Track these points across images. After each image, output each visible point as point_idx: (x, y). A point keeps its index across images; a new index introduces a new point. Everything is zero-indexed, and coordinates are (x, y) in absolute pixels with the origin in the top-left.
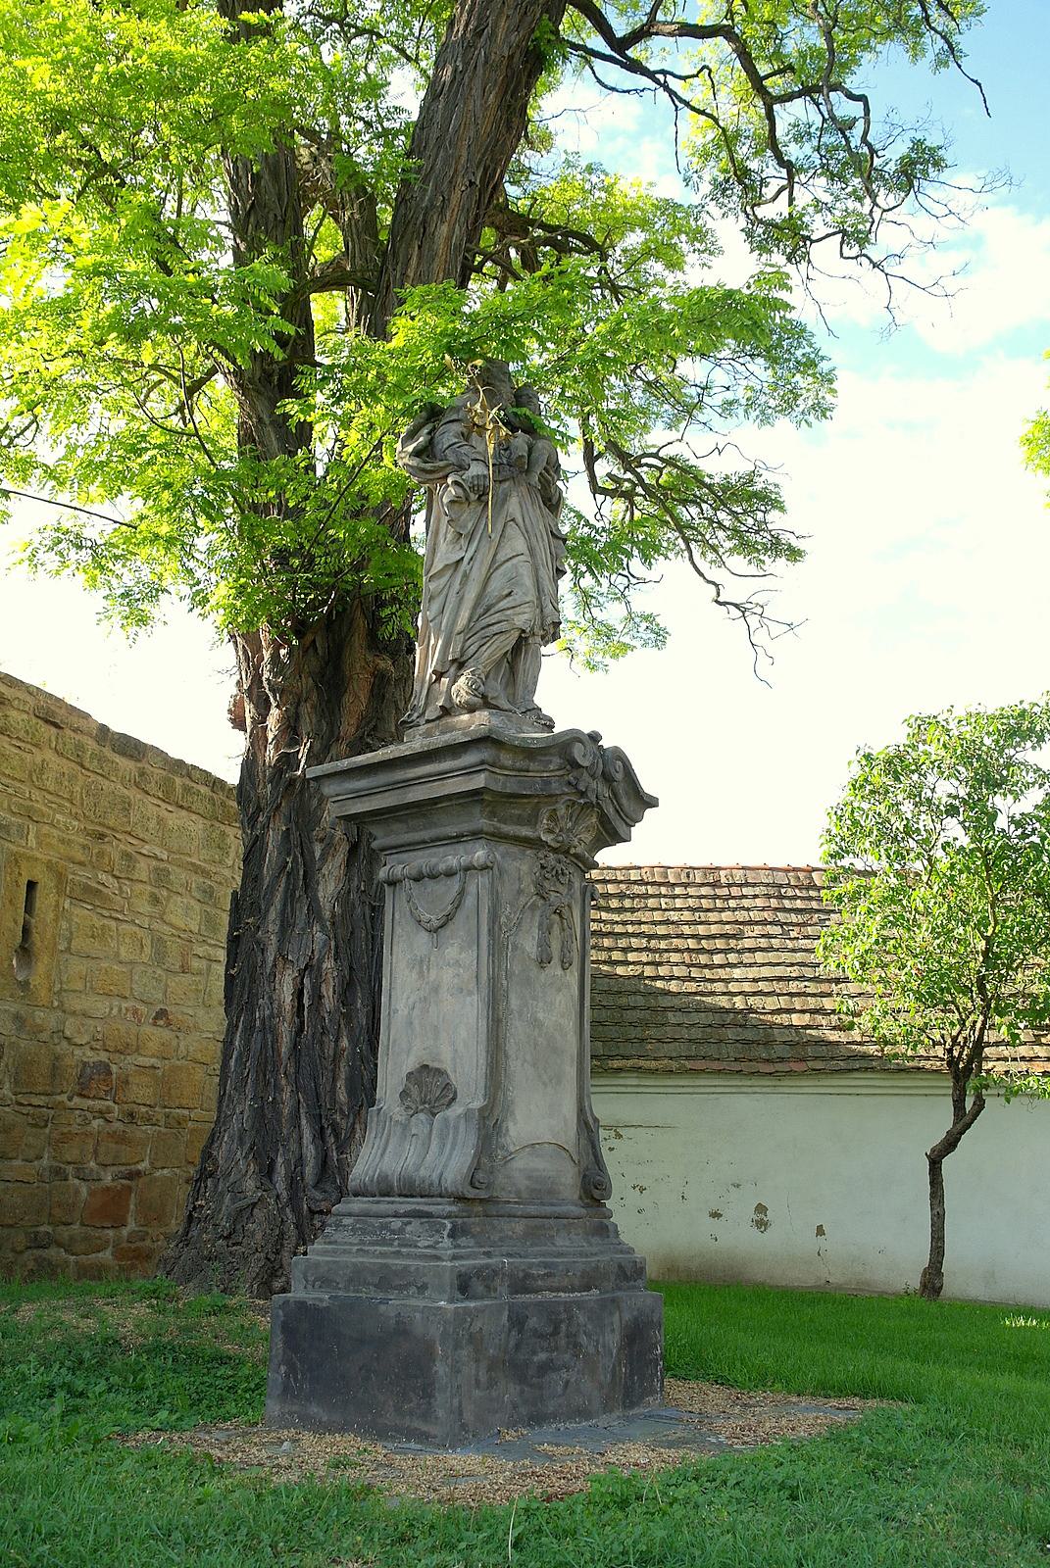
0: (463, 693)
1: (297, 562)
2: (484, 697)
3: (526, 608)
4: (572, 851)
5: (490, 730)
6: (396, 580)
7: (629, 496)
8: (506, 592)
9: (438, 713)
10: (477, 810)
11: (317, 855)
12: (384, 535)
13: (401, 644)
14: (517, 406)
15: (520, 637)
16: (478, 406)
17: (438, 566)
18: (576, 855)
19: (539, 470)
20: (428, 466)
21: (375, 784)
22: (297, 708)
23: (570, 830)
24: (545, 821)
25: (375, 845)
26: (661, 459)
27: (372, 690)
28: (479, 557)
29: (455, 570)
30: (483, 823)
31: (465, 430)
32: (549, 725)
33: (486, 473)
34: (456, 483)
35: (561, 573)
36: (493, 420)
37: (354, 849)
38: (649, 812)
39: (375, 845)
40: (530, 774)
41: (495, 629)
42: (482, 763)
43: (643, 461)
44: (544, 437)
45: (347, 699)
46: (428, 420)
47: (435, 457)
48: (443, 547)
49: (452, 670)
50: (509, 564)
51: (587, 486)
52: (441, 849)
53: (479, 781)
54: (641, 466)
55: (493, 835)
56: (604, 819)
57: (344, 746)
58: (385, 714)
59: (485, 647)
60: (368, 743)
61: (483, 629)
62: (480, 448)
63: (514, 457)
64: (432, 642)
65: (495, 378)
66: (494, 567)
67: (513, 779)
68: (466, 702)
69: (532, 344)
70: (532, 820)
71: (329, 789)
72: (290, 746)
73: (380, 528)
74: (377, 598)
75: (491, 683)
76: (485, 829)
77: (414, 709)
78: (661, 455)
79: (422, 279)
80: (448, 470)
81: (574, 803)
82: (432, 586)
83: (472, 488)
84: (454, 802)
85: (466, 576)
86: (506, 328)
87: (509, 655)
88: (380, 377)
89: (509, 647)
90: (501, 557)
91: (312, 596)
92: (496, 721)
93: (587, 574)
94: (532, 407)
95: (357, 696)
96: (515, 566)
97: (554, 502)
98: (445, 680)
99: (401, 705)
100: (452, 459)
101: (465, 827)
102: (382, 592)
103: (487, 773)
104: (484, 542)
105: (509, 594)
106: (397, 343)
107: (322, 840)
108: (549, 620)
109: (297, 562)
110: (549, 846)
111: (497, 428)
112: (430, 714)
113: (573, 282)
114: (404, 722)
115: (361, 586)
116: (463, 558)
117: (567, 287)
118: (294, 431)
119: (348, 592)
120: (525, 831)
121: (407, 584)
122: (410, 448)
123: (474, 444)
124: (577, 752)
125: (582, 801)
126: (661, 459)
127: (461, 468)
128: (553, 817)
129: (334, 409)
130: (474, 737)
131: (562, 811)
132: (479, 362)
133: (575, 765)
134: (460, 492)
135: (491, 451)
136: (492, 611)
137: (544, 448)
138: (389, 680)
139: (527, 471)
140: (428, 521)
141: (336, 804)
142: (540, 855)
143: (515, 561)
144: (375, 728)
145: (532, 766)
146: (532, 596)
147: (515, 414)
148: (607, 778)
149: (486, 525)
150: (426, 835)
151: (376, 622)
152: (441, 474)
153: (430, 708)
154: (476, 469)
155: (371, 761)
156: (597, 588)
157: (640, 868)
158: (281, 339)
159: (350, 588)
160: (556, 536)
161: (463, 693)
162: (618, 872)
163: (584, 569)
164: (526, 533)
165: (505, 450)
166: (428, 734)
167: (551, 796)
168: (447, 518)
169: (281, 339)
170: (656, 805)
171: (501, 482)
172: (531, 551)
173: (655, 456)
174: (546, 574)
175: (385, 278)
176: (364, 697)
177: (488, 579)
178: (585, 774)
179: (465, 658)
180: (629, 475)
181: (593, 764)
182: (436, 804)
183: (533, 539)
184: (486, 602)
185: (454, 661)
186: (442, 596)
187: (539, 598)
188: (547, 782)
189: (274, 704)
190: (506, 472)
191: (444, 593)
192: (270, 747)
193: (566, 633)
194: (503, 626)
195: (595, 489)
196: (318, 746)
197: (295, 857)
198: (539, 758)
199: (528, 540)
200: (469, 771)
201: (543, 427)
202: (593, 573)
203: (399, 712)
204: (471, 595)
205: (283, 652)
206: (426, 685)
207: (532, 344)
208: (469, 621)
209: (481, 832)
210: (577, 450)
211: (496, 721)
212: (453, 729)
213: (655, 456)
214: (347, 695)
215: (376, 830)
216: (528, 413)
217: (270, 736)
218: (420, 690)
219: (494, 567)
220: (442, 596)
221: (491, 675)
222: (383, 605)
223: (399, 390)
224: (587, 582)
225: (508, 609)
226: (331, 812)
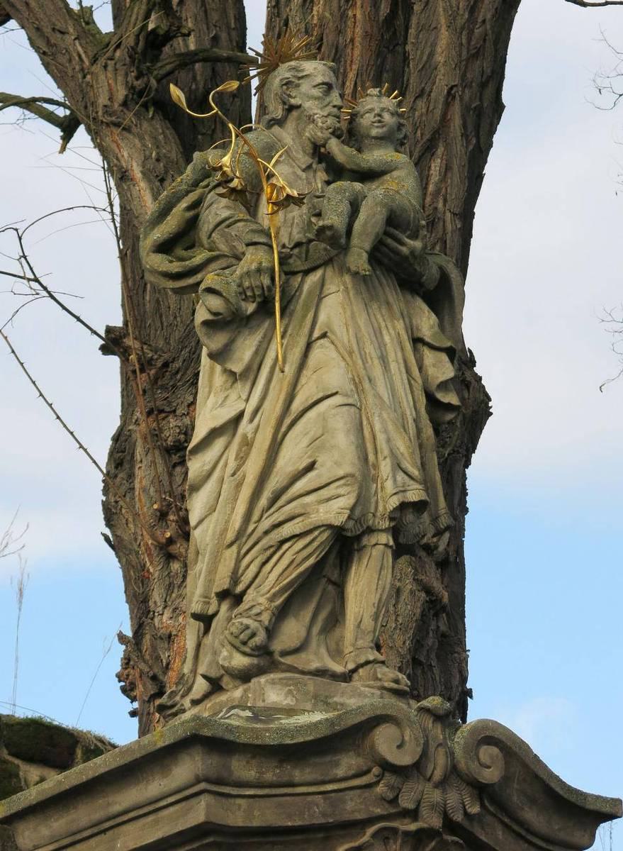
38: (603, 830)
50: (311, 414)
61: (266, 533)
179: (239, 589)
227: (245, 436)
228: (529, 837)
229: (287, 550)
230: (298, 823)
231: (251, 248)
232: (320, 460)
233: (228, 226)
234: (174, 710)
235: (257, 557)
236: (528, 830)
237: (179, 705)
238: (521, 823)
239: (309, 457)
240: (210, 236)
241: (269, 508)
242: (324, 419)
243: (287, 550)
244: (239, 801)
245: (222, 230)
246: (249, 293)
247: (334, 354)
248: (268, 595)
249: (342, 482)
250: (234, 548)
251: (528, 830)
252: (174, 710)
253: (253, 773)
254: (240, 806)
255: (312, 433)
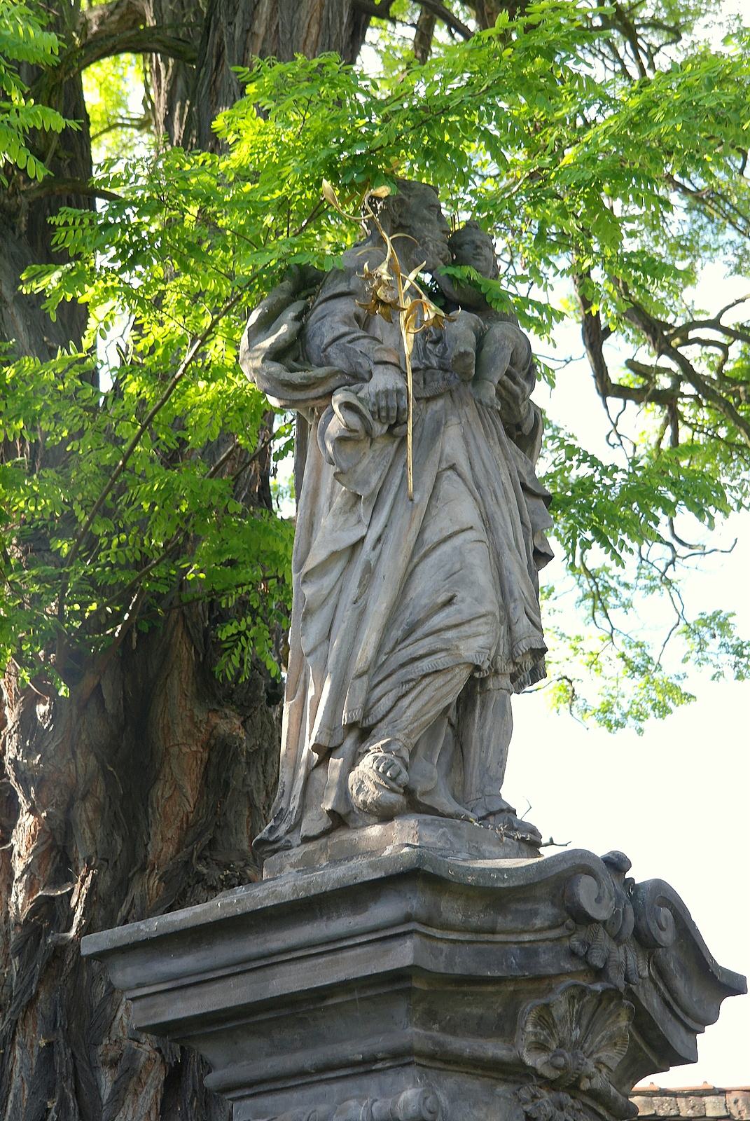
0: (369, 785)
1: (65, 547)
2: (408, 792)
3: (481, 626)
4: (585, 1085)
5: (420, 857)
6: (245, 574)
7: (667, 399)
8: (443, 597)
9: (324, 823)
10: (401, 1008)
11: (106, 1090)
12: (221, 496)
13: (257, 687)
14: (455, 263)
15: (471, 677)
16: (383, 270)
17: (317, 556)
18: (593, 1094)
19: (496, 375)
20: (297, 377)
21: (208, 963)
22: (68, 811)
23: (578, 1044)
24: (530, 1028)
25: (211, 1080)
26: (726, 331)
27: (205, 775)
28: (392, 535)
29: (350, 561)
30: (412, 1034)
31: (361, 311)
32: (532, 842)
33: (400, 385)
34: (347, 406)
35: (542, 557)
36: (412, 292)
37: (174, 1080)
38: (729, 1005)
39: (211, 1080)
40: (499, 938)
41: (425, 665)
42: (408, 919)
43: (692, 334)
44: (503, 318)
45: (161, 792)
46: (294, 295)
47: (308, 360)
48: (325, 522)
49: (349, 743)
50: (446, 548)
51: (591, 383)
52: (336, 1087)
53: (403, 954)
54: (686, 342)
55: (432, 1057)
56: (642, 1022)
57: (154, 882)
58: (231, 817)
59: (406, 701)
60: (198, 874)
61: (403, 666)
62: (389, 342)
63: (451, 354)
64: (311, 692)
65: (414, 215)
66: (419, 552)
67: (467, 949)
68: (377, 803)
69: (477, 153)
70: (505, 1027)
71: (124, 974)
72: (55, 882)
73: (216, 484)
74: (212, 605)
75: (422, 764)
76: (417, 1046)
77: (280, 816)
78: (726, 321)
79: (281, 49)
80: (332, 383)
81: (583, 991)
82: (308, 591)
83: (376, 414)
84: (356, 995)
85: (369, 571)
86: (430, 127)
87: (452, 713)
88: (205, 219)
89: (452, 698)
90: (431, 536)
91: (94, 607)
92: (432, 837)
93: (596, 545)
94: (482, 264)
95: (177, 787)
96: (459, 551)
97: (527, 428)
98: (335, 762)
99: (260, 800)
100: (340, 362)
101: (380, 1043)
102: (222, 593)
103: (416, 938)
104: (401, 508)
105: (450, 602)
106: (241, 155)
107: (113, 1063)
108: (523, 646)
109: (65, 547)
110: (540, 1077)
111: (418, 308)
112: (313, 824)
113: (549, 44)
114: (263, 842)
115: (183, 585)
116: (362, 539)
117: (540, 51)
118: (53, 317)
119: (159, 597)
120: (493, 1049)
121: (265, 579)
122: (267, 343)
123: (378, 333)
124: (585, 893)
125: (598, 987)
126: (726, 331)
127: (357, 377)
128: (545, 1019)
129: (126, 276)
130: (390, 871)
131: (561, 1007)
132: (383, 191)
133: (581, 918)
134: (355, 421)
135: (408, 348)
136: (419, 633)
137: (505, 337)
138: (236, 755)
139: (477, 380)
140: (299, 470)
141: (137, 1004)
142: (524, 1094)
143: (457, 541)
144: (212, 844)
145: (502, 922)
146: (490, 604)
147: (452, 278)
148: (645, 942)
149: (404, 477)
150: (305, 1059)
151: (209, 649)
152: (320, 390)
153: (310, 815)
154: (382, 380)
155: (202, 920)
156: (615, 570)
157: (723, 1092)
158: (36, 141)
159: (164, 590)
160: (530, 490)
161: (369, 785)
162: (682, 1102)
163: (588, 535)
164: (477, 490)
165: (435, 342)
166: (307, 864)
167: (539, 978)
168: (334, 469)
169: (36, 141)
170: (742, 991)
171: (428, 400)
172: (488, 521)
173: (714, 324)
174: (515, 564)
175: (214, 39)
176: (190, 789)
177: (409, 576)
178: (602, 934)
179: (371, 721)
180: (665, 361)
181: (615, 915)
182: (324, 998)
183: (489, 499)
184: (407, 617)
185: (351, 726)
186: (326, 612)
187: (504, 607)
188: (530, 952)
189: (25, 807)
190: (438, 384)
191: (332, 601)
192: (18, 888)
193: (557, 659)
194: (440, 660)
195: (606, 388)
196: (106, 882)
197: (63, 1104)
198: (513, 906)
199: (481, 503)
200: (385, 936)
201: (503, 297)
202: (605, 543)
203: (256, 814)
204: (379, 605)
205: (41, 709)
206: (302, 772)
207: (477, 153)
208: (379, 650)
209: (409, 1051)
210: (569, 334)
211: (432, 837)
212: (351, 852)
213: (714, 324)
214: (159, 786)
215: (211, 1052)
216: (475, 275)
217: (19, 866)
218: (291, 779)
219: (419, 552)
220: (326, 612)
221: (421, 752)
222: (222, 617)
223: (250, 240)
224: (596, 557)
225: (449, 628)
226: (128, 1017)
227: (368, 563)
228: (675, 1007)
229: (428, 685)
230: (497, 974)
231: (381, 367)
232: (459, 596)
233: (350, 342)
234: (276, 846)
235: (391, 690)
236: (675, 1000)
237: (283, 841)
238: (671, 991)
239: (447, 590)
240: (325, 350)
241: (404, 640)
242: (461, 553)
243: (428, 685)
244: (441, 945)
245: (344, 344)
246: (383, 414)
247: (462, 487)
248: (406, 731)
249: (482, 620)
250: (365, 678)
251: (675, 1000)
252: (276, 846)
253: (460, 916)
254: (441, 951)
255: (448, 567)
